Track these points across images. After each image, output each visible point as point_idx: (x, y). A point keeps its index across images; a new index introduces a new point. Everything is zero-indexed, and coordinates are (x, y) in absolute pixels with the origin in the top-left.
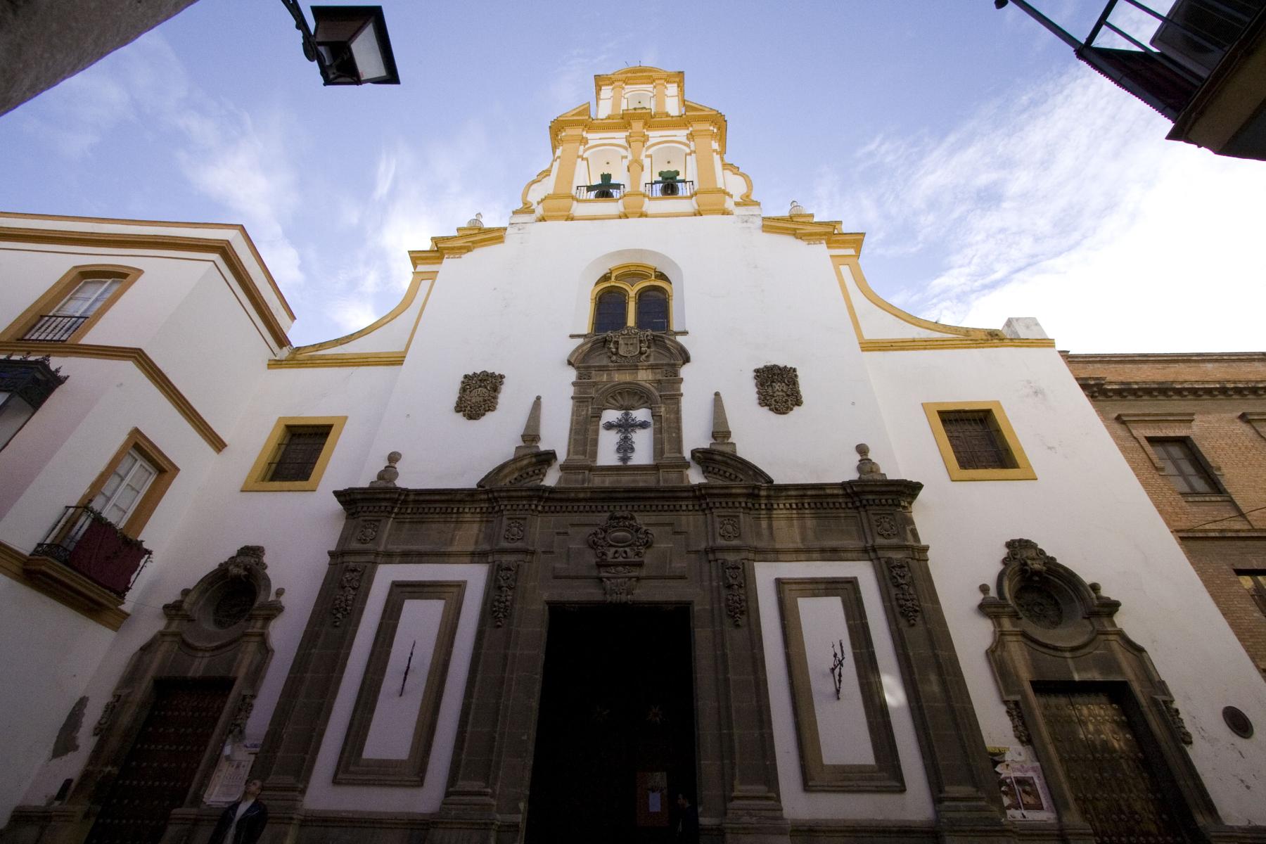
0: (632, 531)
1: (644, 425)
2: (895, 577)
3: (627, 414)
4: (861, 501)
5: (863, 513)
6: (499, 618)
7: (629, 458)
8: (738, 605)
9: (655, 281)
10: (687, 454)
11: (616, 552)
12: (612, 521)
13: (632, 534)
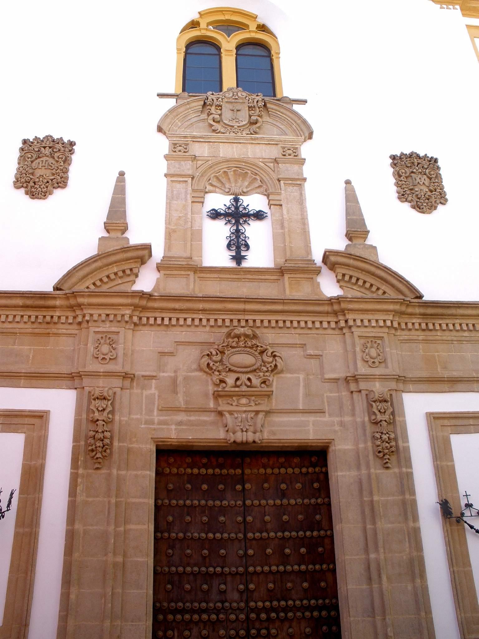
0: (256, 353)
1: (259, 216)
2: (374, 413)
3: (236, 200)
4: (346, 321)
5: (348, 335)
6: (97, 458)
7: (243, 258)
8: (387, 445)
9: (256, 32)
11: (238, 379)
12: (230, 340)
13: (254, 356)
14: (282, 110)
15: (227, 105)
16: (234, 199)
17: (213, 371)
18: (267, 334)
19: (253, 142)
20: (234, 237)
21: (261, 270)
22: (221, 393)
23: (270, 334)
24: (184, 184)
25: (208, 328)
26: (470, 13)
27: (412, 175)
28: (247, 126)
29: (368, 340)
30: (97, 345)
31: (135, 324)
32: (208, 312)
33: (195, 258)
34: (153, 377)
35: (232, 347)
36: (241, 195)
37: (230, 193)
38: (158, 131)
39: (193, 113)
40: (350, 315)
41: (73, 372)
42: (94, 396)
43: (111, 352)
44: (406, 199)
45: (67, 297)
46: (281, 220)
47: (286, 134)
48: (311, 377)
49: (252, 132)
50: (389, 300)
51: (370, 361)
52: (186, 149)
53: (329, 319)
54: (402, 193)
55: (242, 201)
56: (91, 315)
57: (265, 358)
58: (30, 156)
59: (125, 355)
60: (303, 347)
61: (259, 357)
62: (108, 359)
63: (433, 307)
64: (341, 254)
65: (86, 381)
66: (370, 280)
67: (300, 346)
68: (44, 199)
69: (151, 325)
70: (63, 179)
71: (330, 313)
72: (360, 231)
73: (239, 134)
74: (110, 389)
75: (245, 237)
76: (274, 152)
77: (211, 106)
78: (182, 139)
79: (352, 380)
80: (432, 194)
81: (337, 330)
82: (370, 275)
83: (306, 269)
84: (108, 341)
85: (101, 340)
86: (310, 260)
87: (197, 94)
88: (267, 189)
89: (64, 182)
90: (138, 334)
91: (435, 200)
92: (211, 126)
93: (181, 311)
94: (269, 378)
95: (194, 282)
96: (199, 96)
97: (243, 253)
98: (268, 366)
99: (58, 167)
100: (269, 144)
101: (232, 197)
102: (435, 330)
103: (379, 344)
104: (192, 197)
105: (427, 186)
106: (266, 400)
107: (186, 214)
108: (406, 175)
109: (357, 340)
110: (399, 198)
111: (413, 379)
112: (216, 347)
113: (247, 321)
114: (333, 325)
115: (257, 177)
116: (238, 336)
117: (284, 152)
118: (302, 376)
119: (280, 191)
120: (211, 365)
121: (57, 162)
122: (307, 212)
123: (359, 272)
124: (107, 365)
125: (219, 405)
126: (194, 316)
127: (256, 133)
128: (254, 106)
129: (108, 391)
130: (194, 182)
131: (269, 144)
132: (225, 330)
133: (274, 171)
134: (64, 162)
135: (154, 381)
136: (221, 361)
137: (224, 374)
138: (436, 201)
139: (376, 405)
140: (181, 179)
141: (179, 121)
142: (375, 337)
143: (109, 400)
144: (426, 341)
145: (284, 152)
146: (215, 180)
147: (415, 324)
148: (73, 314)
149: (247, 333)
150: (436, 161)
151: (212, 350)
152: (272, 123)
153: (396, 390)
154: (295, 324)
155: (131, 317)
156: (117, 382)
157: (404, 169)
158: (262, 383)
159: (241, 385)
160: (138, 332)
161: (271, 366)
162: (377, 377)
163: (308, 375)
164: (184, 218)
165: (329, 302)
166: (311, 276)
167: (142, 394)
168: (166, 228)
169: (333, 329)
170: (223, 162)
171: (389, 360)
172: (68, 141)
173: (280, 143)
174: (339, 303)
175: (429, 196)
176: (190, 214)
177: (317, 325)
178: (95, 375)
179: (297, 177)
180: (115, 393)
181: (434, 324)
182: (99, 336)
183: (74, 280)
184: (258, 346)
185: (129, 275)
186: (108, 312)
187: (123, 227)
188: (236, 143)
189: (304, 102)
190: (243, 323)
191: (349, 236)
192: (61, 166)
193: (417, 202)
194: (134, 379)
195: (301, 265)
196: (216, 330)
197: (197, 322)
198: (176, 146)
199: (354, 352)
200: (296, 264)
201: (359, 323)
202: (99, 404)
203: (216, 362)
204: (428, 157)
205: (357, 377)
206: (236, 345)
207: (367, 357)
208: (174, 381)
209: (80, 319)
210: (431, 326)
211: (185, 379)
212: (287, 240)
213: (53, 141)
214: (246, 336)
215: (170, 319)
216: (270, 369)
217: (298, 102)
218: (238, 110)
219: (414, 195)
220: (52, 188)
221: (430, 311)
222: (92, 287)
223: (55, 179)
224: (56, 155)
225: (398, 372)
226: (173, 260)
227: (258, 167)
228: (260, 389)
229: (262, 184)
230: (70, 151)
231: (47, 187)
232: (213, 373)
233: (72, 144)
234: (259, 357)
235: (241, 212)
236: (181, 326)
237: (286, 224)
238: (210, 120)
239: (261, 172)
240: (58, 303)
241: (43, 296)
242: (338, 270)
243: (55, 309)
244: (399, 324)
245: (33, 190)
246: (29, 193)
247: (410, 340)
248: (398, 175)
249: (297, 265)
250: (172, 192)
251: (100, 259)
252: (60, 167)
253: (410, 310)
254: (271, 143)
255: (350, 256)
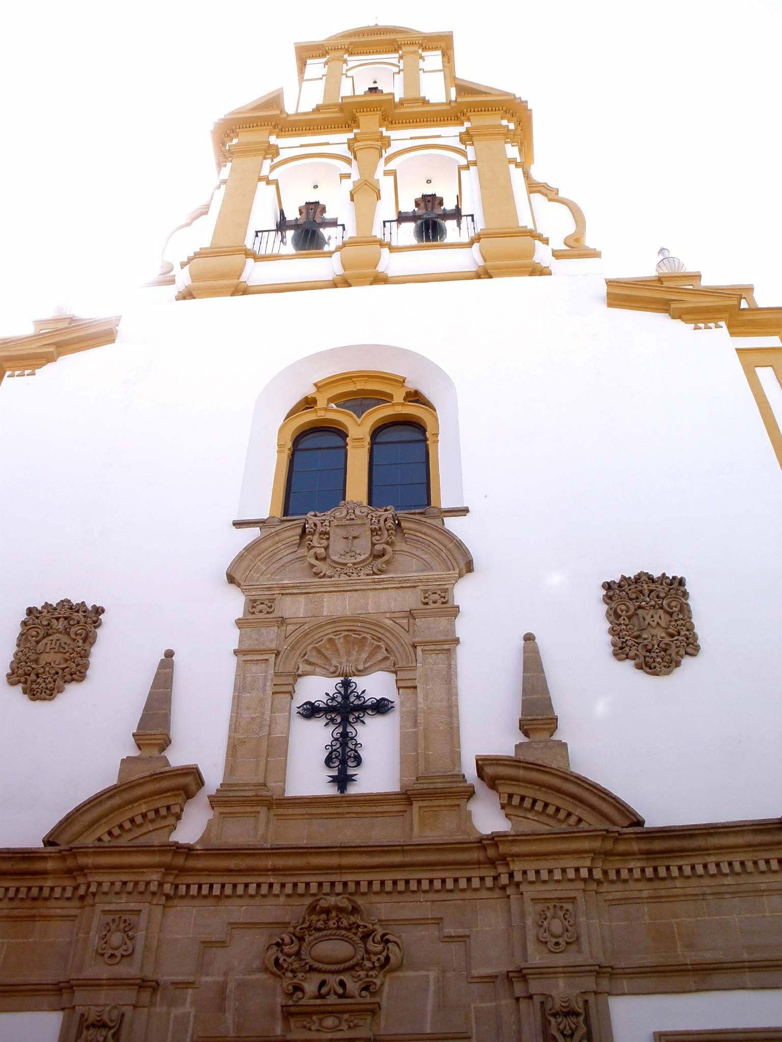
0: (355, 938)
3: (346, 684)
4: (511, 875)
10: (469, 770)
11: (323, 983)
14: (425, 530)
15: (339, 531)
16: (343, 682)
17: (284, 970)
18: (379, 905)
19: (377, 587)
20: (338, 745)
21: (375, 797)
22: (293, 1009)
23: (383, 905)
24: (264, 665)
25: (282, 899)
26: (747, 330)
27: (640, 612)
28: (369, 561)
29: (547, 905)
30: (104, 933)
31: (168, 897)
32: (282, 873)
33: (271, 784)
34: (188, 985)
35: (319, 930)
36: (354, 675)
37: (336, 674)
38: (229, 583)
39: (284, 548)
40: (517, 863)
41: (60, 980)
42: (87, 1023)
43: (126, 944)
44: (627, 655)
45: (62, 856)
46: (415, 711)
47: (432, 567)
48: (449, 975)
49: (376, 570)
50: (580, 834)
51: (551, 941)
52: (270, 607)
53: (483, 873)
54: (620, 645)
55: (354, 684)
56: (100, 884)
57: (371, 946)
58: (34, 633)
59: (147, 948)
60: (438, 923)
61: (359, 945)
62: (119, 957)
63: (663, 838)
64: (502, 762)
65: (80, 996)
66: (555, 800)
67: (433, 921)
68: (50, 700)
69: (193, 897)
70: (79, 668)
71: (484, 863)
72: (542, 719)
73: (355, 576)
74: (115, 1007)
75: (356, 744)
76: (410, 600)
77: (313, 534)
78: (266, 593)
79: (518, 977)
80: (672, 641)
81: (497, 890)
82: (555, 793)
83: (446, 790)
84: (122, 926)
85: (111, 924)
86: (457, 776)
87: (294, 518)
88: (396, 662)
89: (80, 672)
90: (172, 912)
91: (677, 650)
92: (312, 566)
93: (240, 872)
94: (374, 980)
95: (268, 822)
96: (298, 520)
97: (350, 772)
98: (374, 958)
99: (73, 649)
100: (402, 587)
101: (339, 680)
102: (670, 877)
103: (567, 910)
104: (274, 685)
105: (663, 628)
106: (369, 1018)
107: (263, 713)
108: (629, 614)
109: (530, 907)
110: (615, 655)
111: (627, 971)
112: (291, 930)
113: (345, 884)
114: (489, 882)
115: (382, 644)
116: (327, 911)
117: (425, 598)
118: (432, 975)
119: (414, 664)
120: (281, 961)
121: (74, 640)
122: (457, 695)
123: (536, 789)
124: (115, 967)
125: (290, 1031)
126: (261, 879)
127: (382, 571)
128: (380, 528)
129: (110, 1012)
130: (279, 660)
131: (402, 587)
132: (308, 901)
133: (408, 632)
134: (85, 641)
135: (190, 991)
136: (298, 953)
137: (300, 975)
138: (678, 652)
139: (556, 1022)
140: (259, 657)
141: (262, 564)
142: (561, 899)
143: (110, 1028)
144: (656, 899)
145: (425, 598)
146: (314, 653)
147: (634, 871)
148: (73, 883)
149: (341, 905)
150: (681, 582)
151: (283, 936)
152: (410, 553)
153: (596, 993)
154: (425, 885)
155: (161, 885)
156: (128, 996)
157: (625, 604)
158: (363, 989)
159: (328, 993)
160: (172, 909)
161: (379, 959)
162: (561, 969)
163: (444, 972)
164: (259, 720)
165: (479, 845)
166: (456, 802)
167: (169, 1014)
168: (230, 737)
169: (490, 889)
170: (327, 624)
171: (584, 940)
172: (92, 607)
173: (420, 584)
174: (496, 845)
175: (666, 644)
176: (269, 712)
177: (463, 884)
178: (94, 984)
179: (443, 638)
180: (123, 1015)
181: (668, 868)
182: (109, 918)
183: (76, 828)
184: (358, 926)
185: (164, 817)
186: (125, 878)
187: (160, 739)
188: (350, 591)
189: (464, 511)
190: (339, 888)
191: (525, 728)
192: (78, 647)
193: (645, 657)
194: (158, 989)
195: (439, 785)
196: (296, 901)
197: (264, 890)
198: (255, 604)
199: (523, 928)
200: (432, 783)
201: (531, 876)
202: (93, 1036)
203: (289, 956)
204: (668, 578)
205: (524, 971)
206: (322, 926)
207: (545, 935)
208: (222, 989)
209: (82, 891)
210: (662, 872)
211: (239, 985)
212: (422, 743)
213: (71, 608)
214: (341, 910)
215: (223, 886)
216: (377, 964)
217: (453, 513)
218: (355, 538)
219: (640, 646)
220: (61, 683)
221: (657, 845)
222: (106, 838)
223: (67, 667)
224: (73, 629)
225: (601, 959)
226: (235, 788)
227: (382, 627)
228: (359, 1000)
229: (388, 655)
230: (95, 622)
231: (55, 681)
232: (284, 974)
233: (98, 611)
234: (359, 945)
235: (352, 703)
236: (240, 896)
237: (421, 719)
238: (310, 557)
239: (388, 634)
240: (50, 865)
241: (26, 855)
242: (501, 789)
243: (46, 876)
244: (605, 873)
245: (34, 686)
246: (28, 691)
247: (625, 899)
248: (614, 615)
249: (432, 786)
250: (245, 678)
251: (118, 792)
252: (77, 649)
253: (622, 847)
254: (404, 585)
255: (519, 764)
